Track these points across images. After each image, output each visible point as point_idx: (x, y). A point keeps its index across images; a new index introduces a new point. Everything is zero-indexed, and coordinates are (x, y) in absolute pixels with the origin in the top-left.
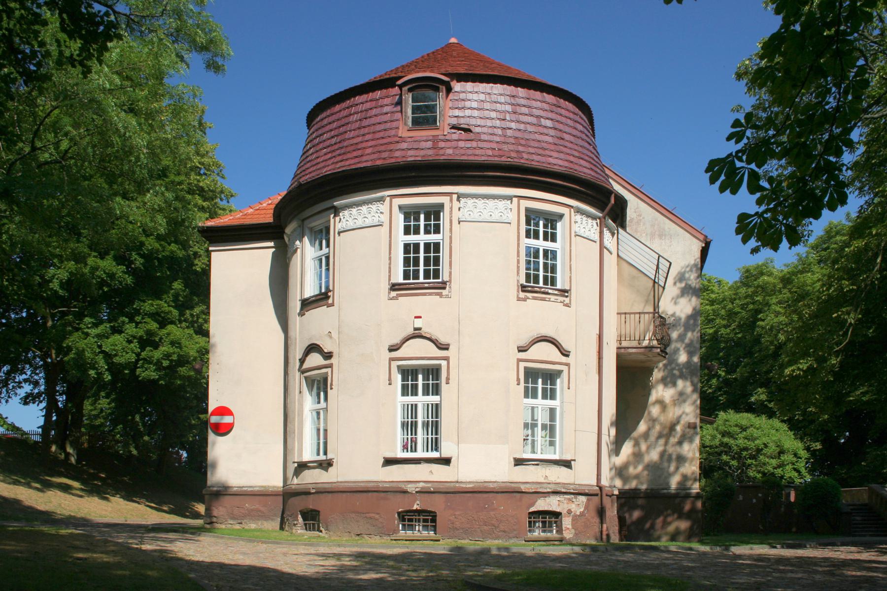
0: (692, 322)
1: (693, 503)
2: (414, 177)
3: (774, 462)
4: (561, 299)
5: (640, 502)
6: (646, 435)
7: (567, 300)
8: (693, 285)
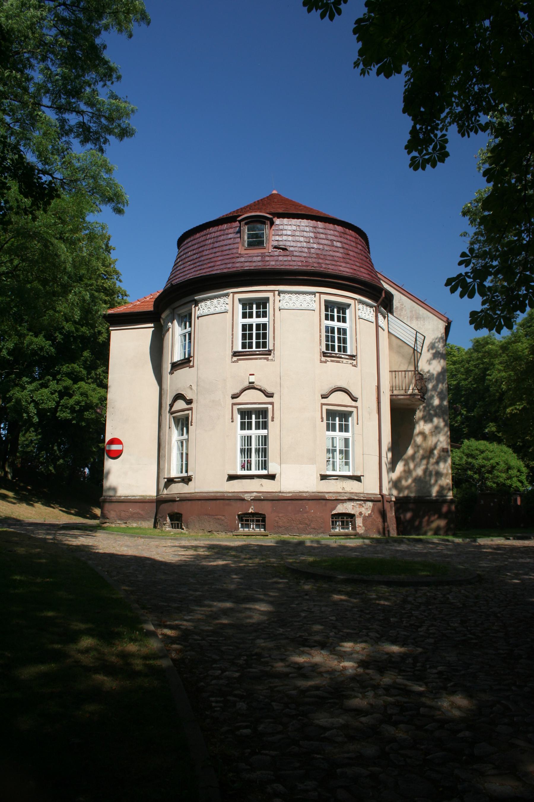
0: (441, 377)
5: (411, 506)
6: (413, 458)
7: (354, 362)
8: (441, 352)
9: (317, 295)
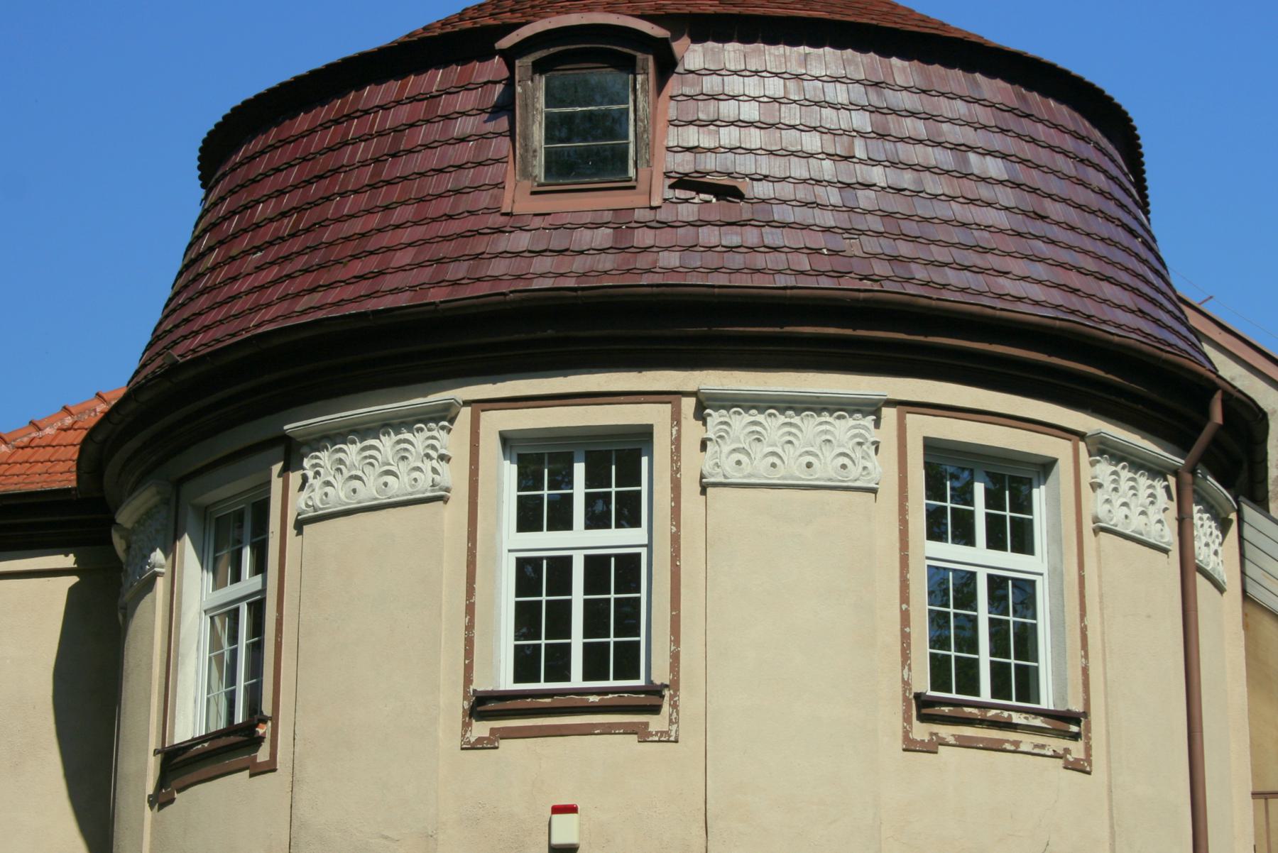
4: (1057, 744)
9: (889, 414)
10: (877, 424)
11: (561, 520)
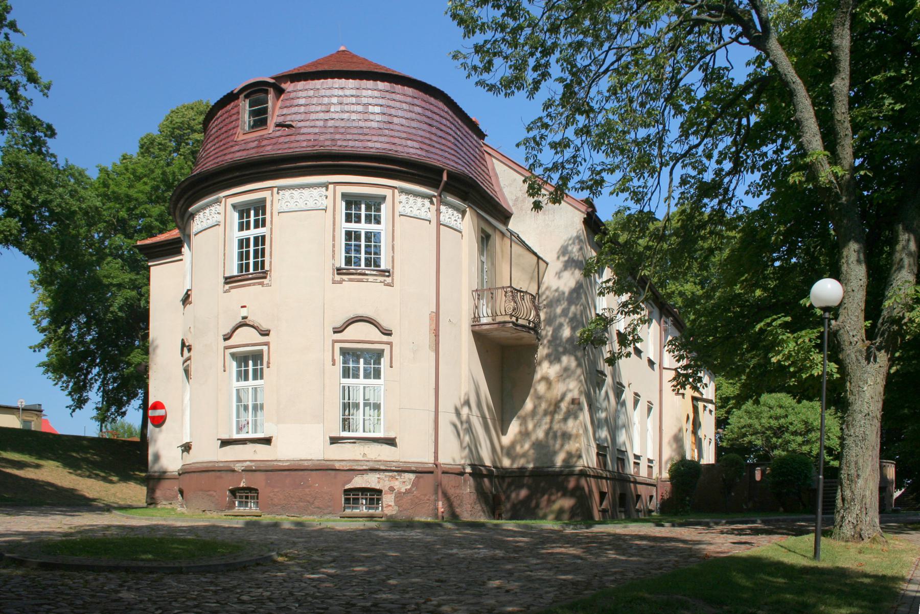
0: (575, 295)
1: (578, 481)
2: (237, 177)
3: (799, 439)
4: (382, 279)
5: (526, 480)
6: (534, 413)
7: (389, 280)
8: (576, 258)
9: (331, 186)
10: (327, 190)
11: (358, 220)
